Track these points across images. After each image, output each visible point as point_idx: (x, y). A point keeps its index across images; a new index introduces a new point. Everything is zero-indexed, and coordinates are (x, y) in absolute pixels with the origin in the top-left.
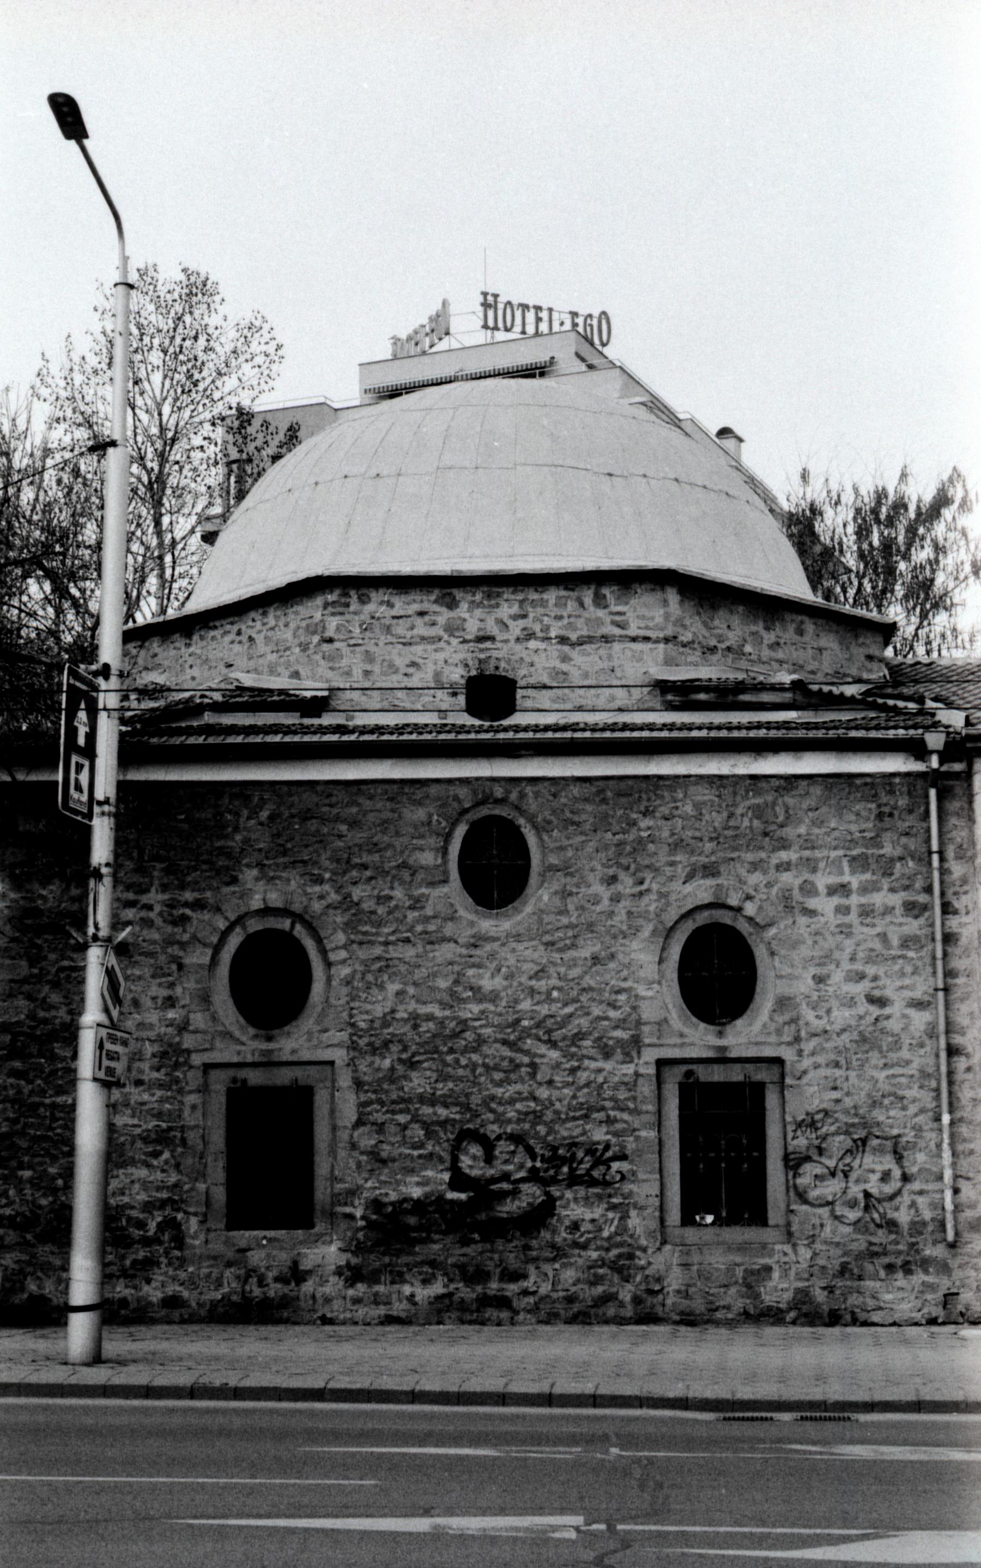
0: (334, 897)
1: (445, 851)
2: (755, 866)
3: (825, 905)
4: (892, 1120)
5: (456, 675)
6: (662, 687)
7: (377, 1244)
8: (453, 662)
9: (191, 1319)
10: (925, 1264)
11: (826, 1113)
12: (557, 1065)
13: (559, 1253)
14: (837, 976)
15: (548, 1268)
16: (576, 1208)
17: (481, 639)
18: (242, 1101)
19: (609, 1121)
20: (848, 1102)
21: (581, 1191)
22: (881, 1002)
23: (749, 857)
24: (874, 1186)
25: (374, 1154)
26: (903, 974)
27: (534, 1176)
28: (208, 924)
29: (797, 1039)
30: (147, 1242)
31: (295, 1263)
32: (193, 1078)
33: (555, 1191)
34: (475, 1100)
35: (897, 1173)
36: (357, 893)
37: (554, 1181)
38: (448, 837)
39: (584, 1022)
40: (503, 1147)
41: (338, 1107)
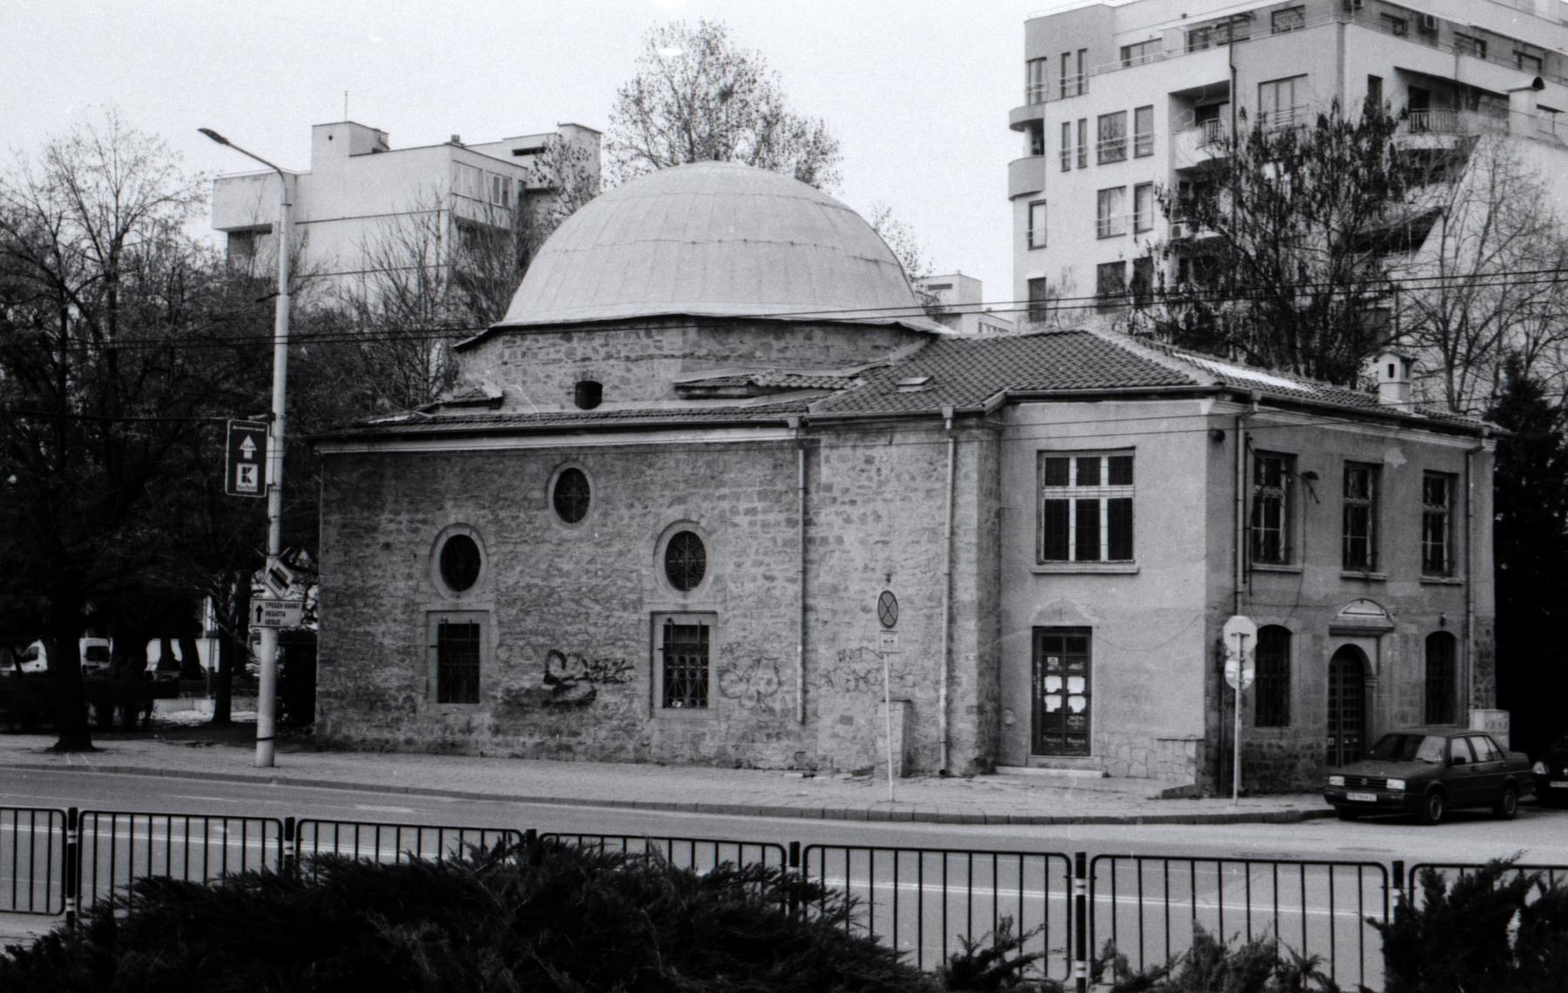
0: (490, 517)
1: (546, 490)
2: (706, 498)
3: (742, 520)
4: (774, 649)
5: (570, 381)
6: (678, 387)
7: (509, 713)
8: (567, 375)
9: (417, 752)
10: (789, 734)
11: (739, 644)
12: (599, 614)
13: (598, 722)
14: (749, 563)
15: (592, 730)
16: (606, 696)
17: (584, 360)
18: (446, 630)
19: (626, 647)
20: (751, 638)
21: (610, 686)
22: (770, 578)
23: (703, 492)
24: (762, 688)
25: (507, 662)
26: (783, 562)
27: (586, 677)
28: (428, 533)
29: (725, 601)
30: (399, 708)
31: (469, 723)
32: (421, 619)
33: (596, 686)
34: (558, 632)
35: (775, 680)
36: (502, 514)
37: (596, 680)
38: (548, 481)
39: (613, 589)
40: (571, 661)
41: (490, 638)
